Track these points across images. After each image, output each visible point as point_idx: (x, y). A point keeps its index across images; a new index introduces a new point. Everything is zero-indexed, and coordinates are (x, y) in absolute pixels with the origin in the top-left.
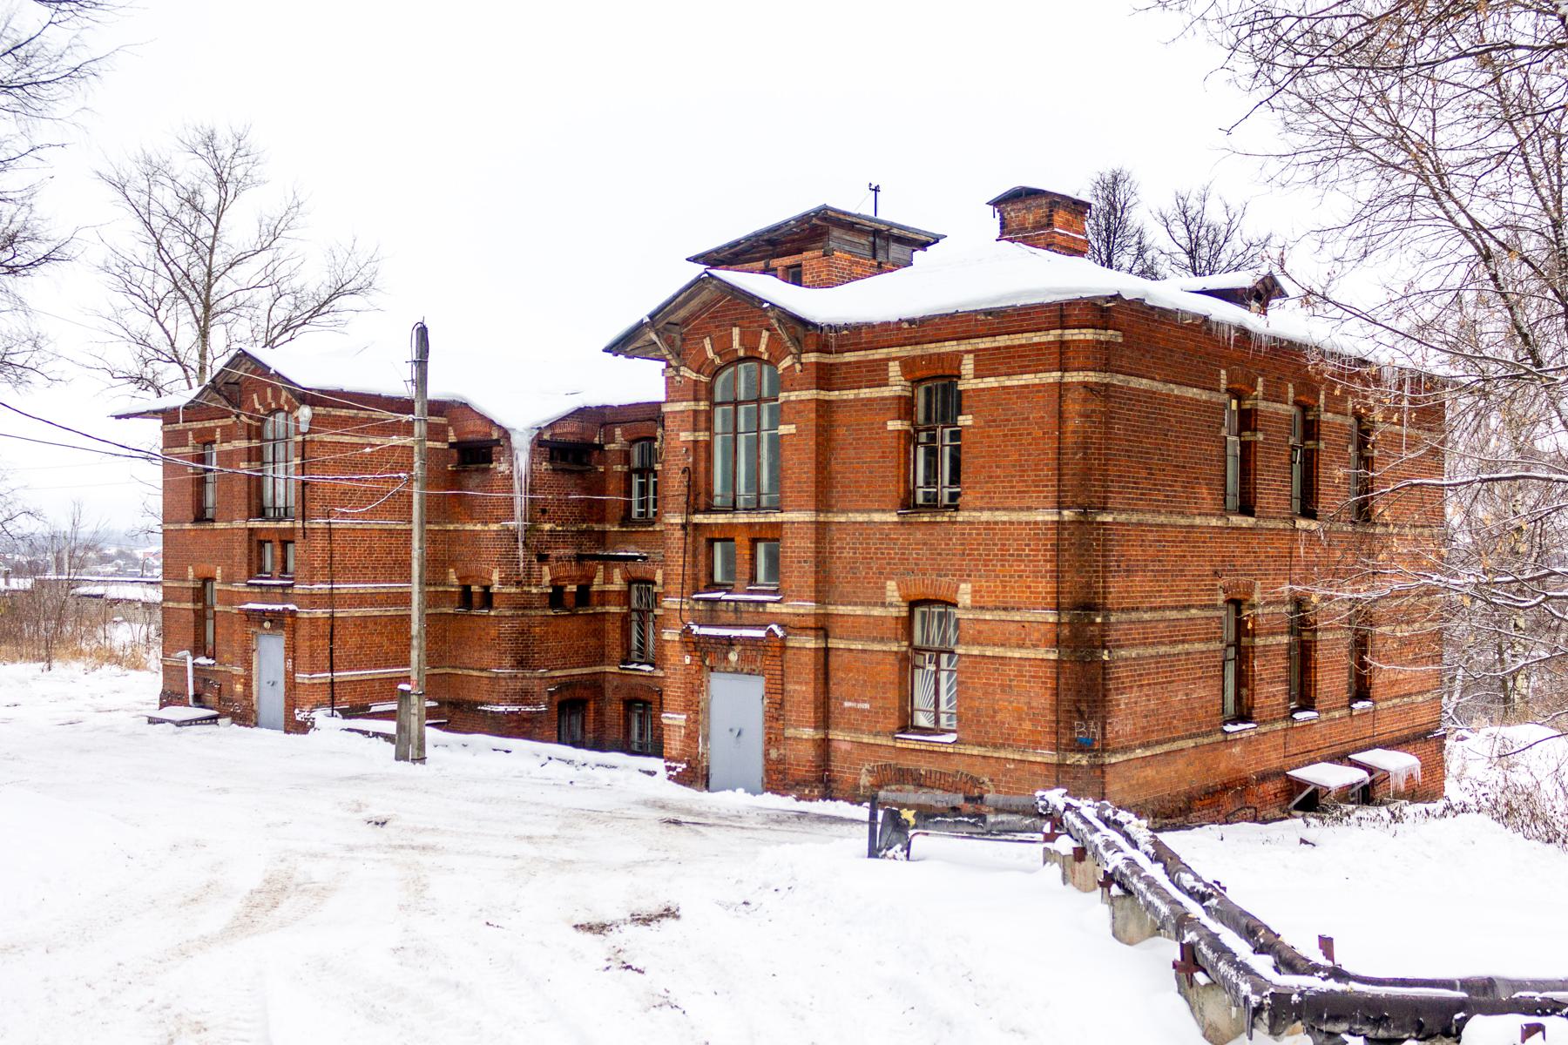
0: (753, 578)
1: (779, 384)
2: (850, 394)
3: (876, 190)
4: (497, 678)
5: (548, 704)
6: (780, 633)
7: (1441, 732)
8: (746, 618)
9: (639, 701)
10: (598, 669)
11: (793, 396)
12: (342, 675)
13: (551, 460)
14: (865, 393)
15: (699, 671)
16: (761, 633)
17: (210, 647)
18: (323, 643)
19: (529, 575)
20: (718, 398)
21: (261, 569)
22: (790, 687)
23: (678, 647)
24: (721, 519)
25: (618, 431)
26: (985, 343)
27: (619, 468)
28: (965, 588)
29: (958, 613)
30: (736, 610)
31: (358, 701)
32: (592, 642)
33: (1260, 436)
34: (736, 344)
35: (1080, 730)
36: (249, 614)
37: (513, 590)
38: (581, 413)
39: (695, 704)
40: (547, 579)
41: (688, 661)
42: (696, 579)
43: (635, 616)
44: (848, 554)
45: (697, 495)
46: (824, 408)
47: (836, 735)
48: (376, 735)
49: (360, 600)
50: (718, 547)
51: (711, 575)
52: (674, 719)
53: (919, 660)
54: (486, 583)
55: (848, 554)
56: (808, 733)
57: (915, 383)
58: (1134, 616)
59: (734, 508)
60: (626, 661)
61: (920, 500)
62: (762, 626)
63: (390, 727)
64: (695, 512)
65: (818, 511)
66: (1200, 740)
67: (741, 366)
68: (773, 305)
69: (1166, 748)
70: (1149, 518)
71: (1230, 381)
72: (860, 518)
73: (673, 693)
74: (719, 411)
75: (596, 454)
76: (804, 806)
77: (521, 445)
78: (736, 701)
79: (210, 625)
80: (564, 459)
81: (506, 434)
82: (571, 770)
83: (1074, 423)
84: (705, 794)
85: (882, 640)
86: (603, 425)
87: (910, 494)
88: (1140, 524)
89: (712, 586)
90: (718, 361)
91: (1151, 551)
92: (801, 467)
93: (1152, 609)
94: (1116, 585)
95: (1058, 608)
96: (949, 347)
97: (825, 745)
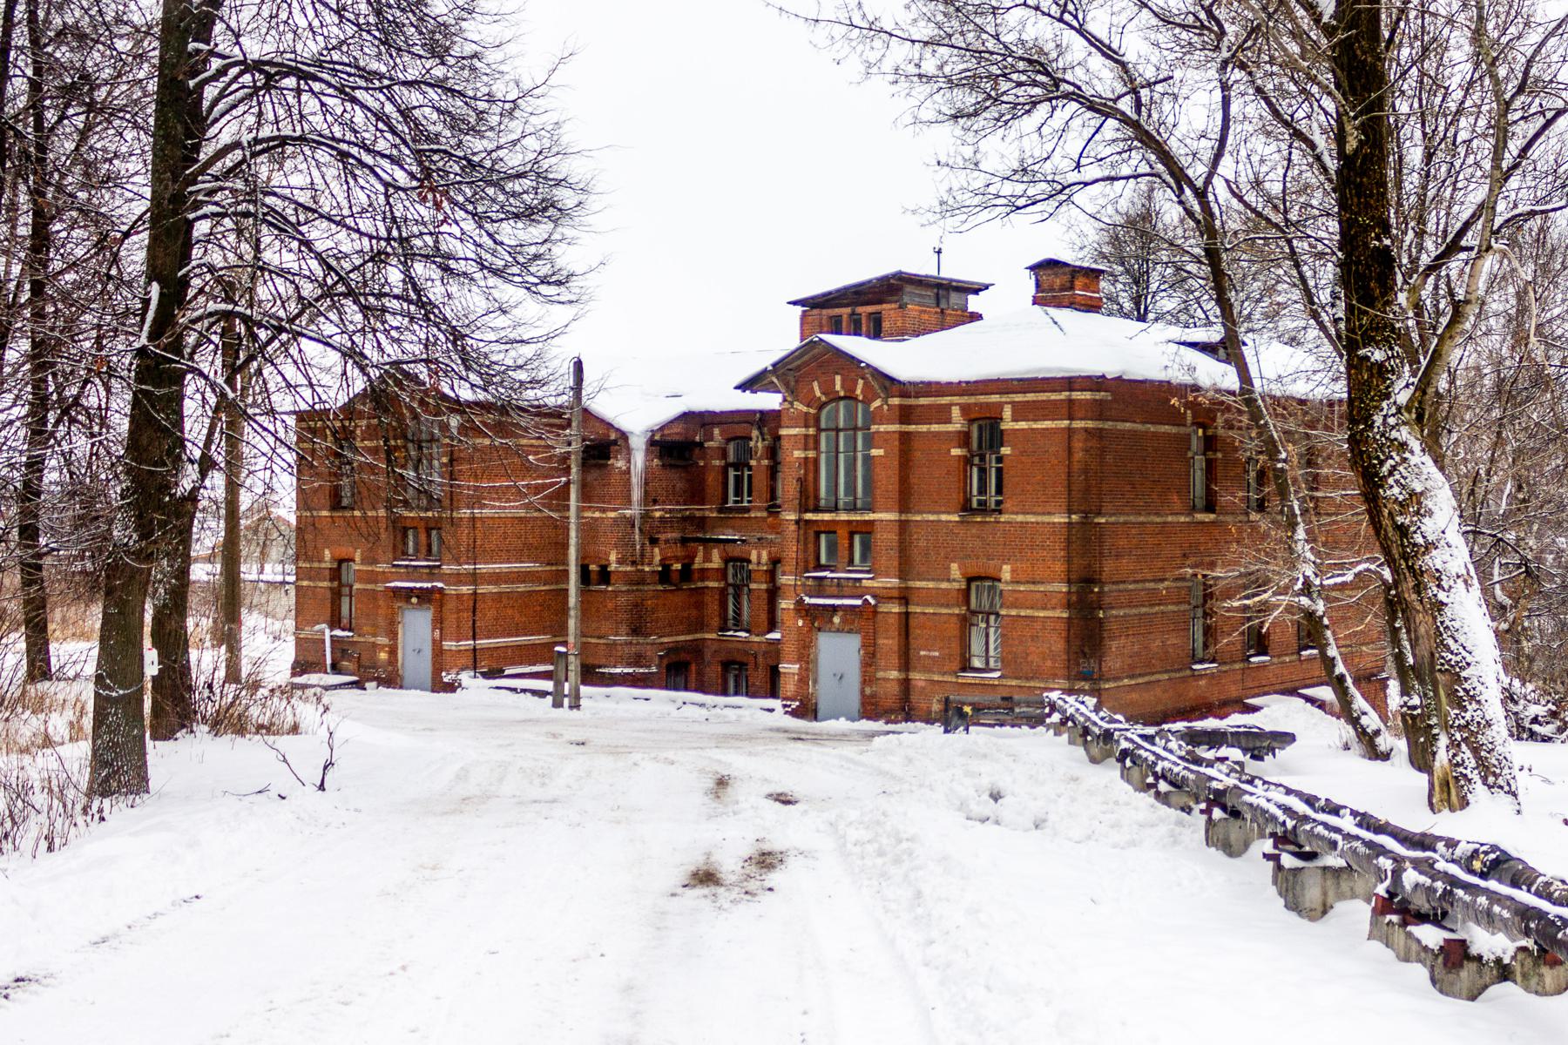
0: (851, 562)
1: (871, 418)
2: (924, 428)
3: (939, 252)
4: (615, 643)
5: (658, 666)
6: (872, 602)
7: (1384, 675)
8: (847, 591)
9: (734, 662)
10: (698, 636)
11: (882, 428)
12: (483, 642)
13: (661, 457)
14: (935, 428)
15: (810, 631)
16: (858, 602)
17: (345, 621)
18: (467, 615)
19: (642, 555)
20: (823, 425)
21: (405, 553)
22: (880, 641)
23: (792, 613)
24: (827, 517)
25: (716, 431)
26: (1019, 398)
27: (717, 463)
28: (1006, 568)
29: (1001, 586)
30: (838, 585)
31: (495, 666)
32: (694, 612)
33: (1219, 455)
34: (838, 387)
35: (1084, 666)
36: (396, 590)
38: (687, 416)
39: (806, 655)
40: (657, 558)
41: (800, 623)
42: (806, 561)
43: (731, 590)
44: (922, 543)
45: (807, 498)
46: (905, 438)
47: (914, 675)
48: (524, 691)
49: (496, 578)
50: (823, 537)
51: (818, 558)
52: (789, 668)
53: (974, 620)
54: (603, 562)
55: (922, 543)
56: (894, 674)
57: (971, 421)
58: (1121, 586)
59: (836, 509)
60: (724, 628)
61: (975, 505)
62: (860, 597)
63: (548, 685)
64: (807, 511)
65: (901, 512)
66: (1173, 675)
67: (842, 404)
68: (868, 366)
69: (1146, 679)
70: (1132, 518)
71: (1194, 417)
72: (932, 517)
73: (789, 648)
74: (823, 435)
75: (697, 451)
76: (891, 727)
77: (638, 444)
78: (839, 654)
79: (345, 602)
80: (670, 455)
81: (624, 436)
82: (703, 711)
83: (1079, 455)
84: (815, 724)
85: (947, 606)
86: (703, 425)
87: (968, 501)
88: (1125, 523)
89: (819, 567)
90: (824, 399)
91: (1134, 541)
92: (888, 479)
93: (1136, 582)
94: (1109, 566)
95: (1069, 582)
96: (995, 398)
97: (906, 684)
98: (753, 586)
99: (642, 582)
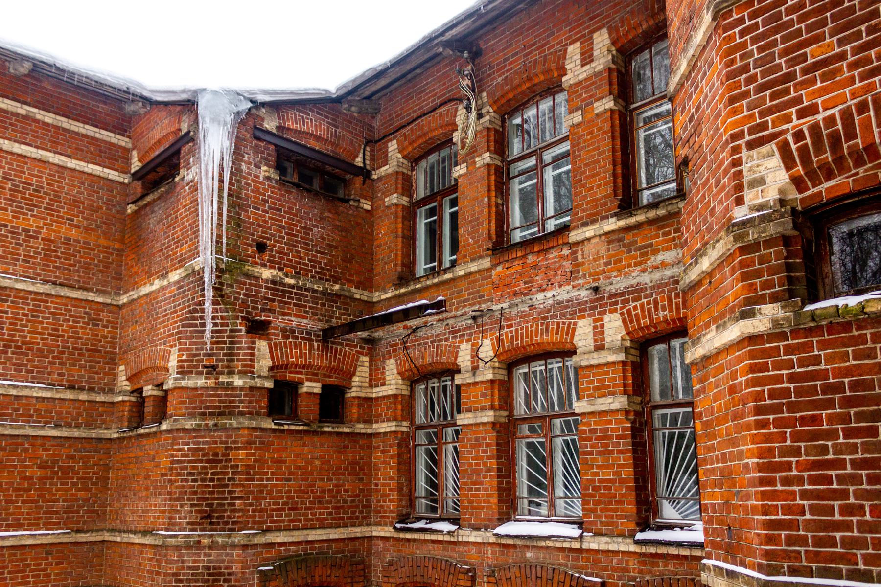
10: (357, 531)
32: (348, 483)
37: (201, 382)
40: (264, 363)
43: (421, 437)
98: (463, 419)
99: (227, 410)
